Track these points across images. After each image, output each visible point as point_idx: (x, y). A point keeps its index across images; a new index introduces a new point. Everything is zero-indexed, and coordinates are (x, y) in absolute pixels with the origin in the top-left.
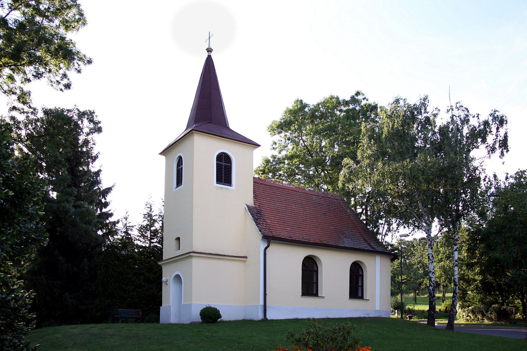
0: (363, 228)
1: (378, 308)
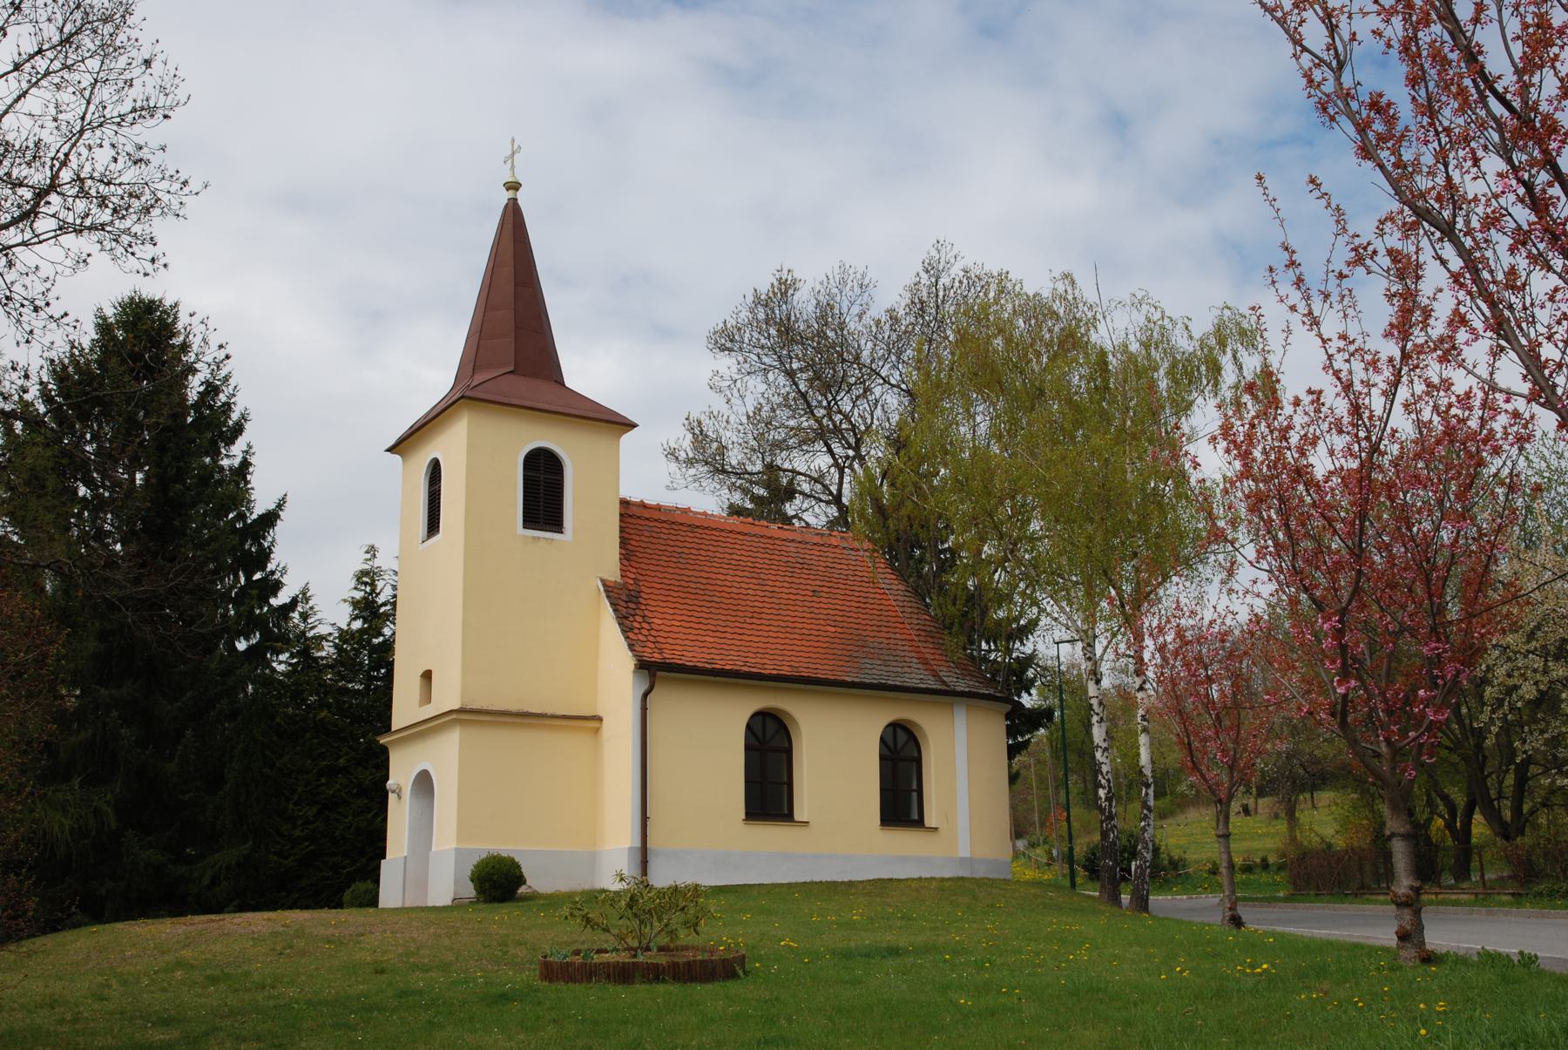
0: (922, 628)
1: (964, 851)
